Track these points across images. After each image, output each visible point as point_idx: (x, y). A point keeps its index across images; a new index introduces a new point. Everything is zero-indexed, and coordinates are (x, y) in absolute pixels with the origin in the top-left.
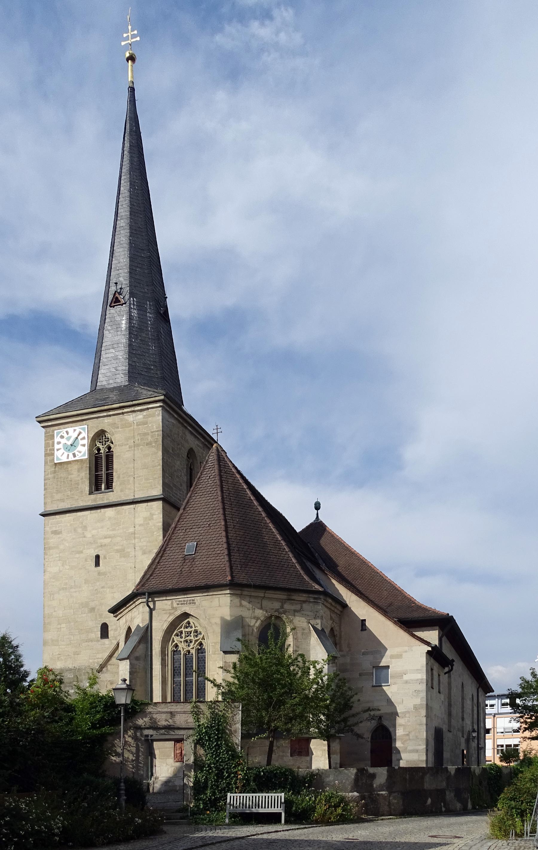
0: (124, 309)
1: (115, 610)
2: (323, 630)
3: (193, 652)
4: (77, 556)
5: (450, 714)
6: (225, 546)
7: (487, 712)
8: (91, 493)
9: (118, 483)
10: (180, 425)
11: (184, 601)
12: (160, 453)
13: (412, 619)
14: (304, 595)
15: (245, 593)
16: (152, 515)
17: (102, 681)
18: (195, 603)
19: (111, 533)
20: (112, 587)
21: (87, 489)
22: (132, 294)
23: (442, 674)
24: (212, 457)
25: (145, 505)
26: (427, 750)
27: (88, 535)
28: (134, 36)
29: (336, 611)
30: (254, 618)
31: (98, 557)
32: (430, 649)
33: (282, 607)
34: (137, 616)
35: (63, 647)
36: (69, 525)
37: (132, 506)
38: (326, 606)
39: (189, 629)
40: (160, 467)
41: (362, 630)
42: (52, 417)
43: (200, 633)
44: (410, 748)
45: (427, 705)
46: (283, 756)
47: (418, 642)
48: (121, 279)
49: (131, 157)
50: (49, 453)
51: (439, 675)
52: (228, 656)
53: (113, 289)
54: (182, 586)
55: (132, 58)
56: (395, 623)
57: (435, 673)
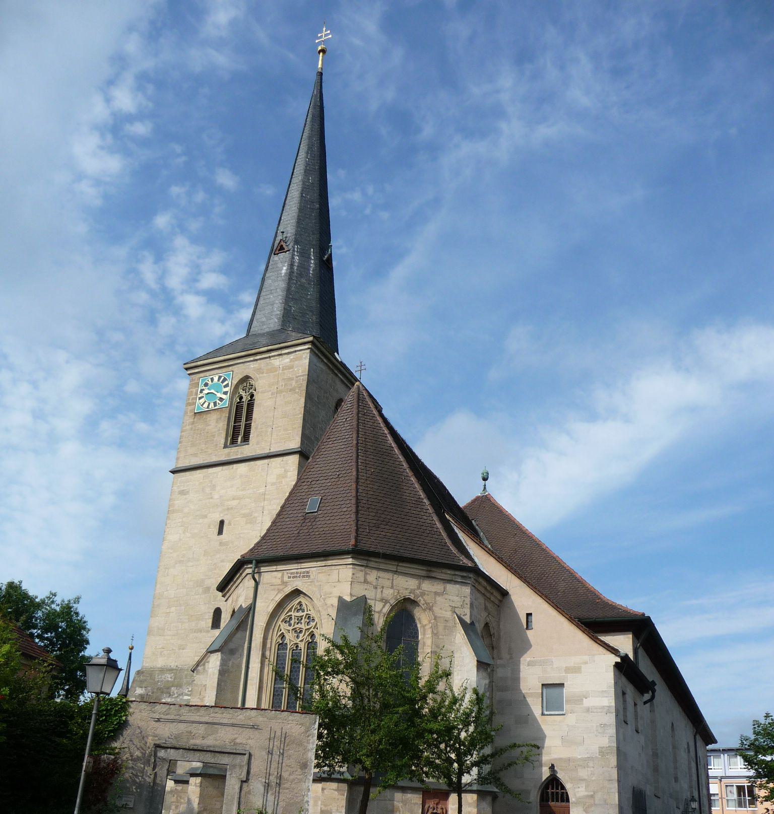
0: (287, 255)
2: (472, 623)
3: (302, 645)
4: (201, 521)
5: (656, 769)
6: (354, 501)
7: (710, 775)
8: (225, 446)
10: (328, 371)
11: (297, 573)
12: (303, 400)
13: (598, 621)
14: (449, 572)
15: (372, 564)
16: (286, 471)
18: (309, 576)
21: (223, 441)
22: (296, 242)
24: (350, 397)
27: (216, 496)
28: (326, 35)
29: (492, 598)
30: (382, 600)
31: (222, 523)
32: (619, 660)
33: (419, 587)
35: (169, 638)
37: (266, 461)
38: (478, 590)
39: (300, 614)
40: (301, 416)
41: (527, 628)
45: (618, 748)
47: (601, 649)
48: (289, 229)
51: (635, 704)
53: (279, 238)
56: (571, 619)
57: (630, 698)
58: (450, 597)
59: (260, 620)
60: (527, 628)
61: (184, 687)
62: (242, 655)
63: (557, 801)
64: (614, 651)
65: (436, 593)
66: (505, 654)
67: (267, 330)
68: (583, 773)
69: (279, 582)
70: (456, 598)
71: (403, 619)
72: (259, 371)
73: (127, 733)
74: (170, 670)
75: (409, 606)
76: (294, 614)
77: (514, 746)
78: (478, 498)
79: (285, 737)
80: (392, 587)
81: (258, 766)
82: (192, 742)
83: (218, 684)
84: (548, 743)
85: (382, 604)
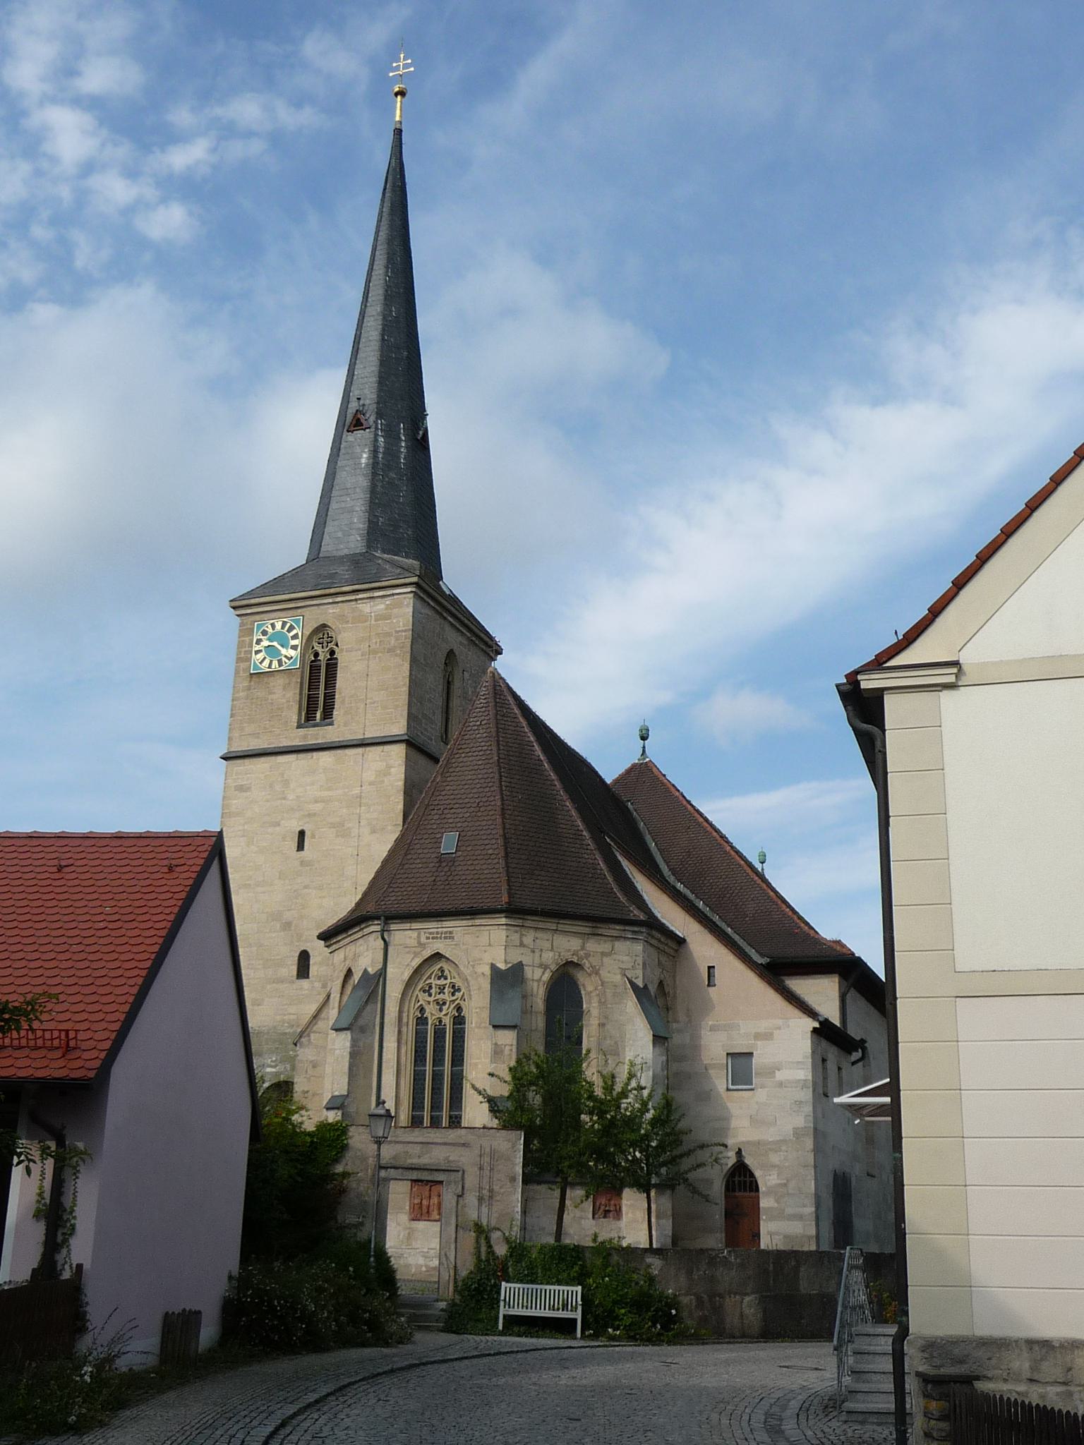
1: (327, 936)
2: (646, 986)
4: (270, 830)
6: (501, 841)
9: (342, 711)
12: (407, 666)
15: (528, 923)
17: (301, 1061)
19: (326, 793)
20: (320, 888)
21: (295, 718)
22: (380, 415)
23: (846, 1066)
25: (380, 748)
26: (817, 1218)
27: (291, 797)
28: (406, 66)
30: (541, 966)
32: (817, 1025)
33: (583, 948)
34: (364, 952)
36: (262, 776)
40: (406, 689)
41: (709, 985)
42: (253, 601)
43: (459, 990)
44: (789, 1211)
45: (815, 1129)
46: (581, 1218)
48: (366, 391)
49: (392, 221)
50: (243, 657)
51: (839, 1069)
52: (500, 1033)
54: (435, 907)
55: (402, 93)
57: (832, 1066)
58: (620, 957)
59: (394, 991)
60: (709, 985)
62: (373, 1033)
63: (745, 1190)
64: (810, 1012)
65: (603, 954)
66: (682, 1017)
67: (346, 552)
68: (775, 1158)
69: (414, 942)
70: (626, 958)
71: (565, 989)
72: (342, 618)
73: (349, 1155)
75: (571, 970)
76: (434, 982)
77: (702, 1147)
78: (634, 766)
79: (493, 1153)
80: (552, 950)
81: (471, 1181)
82: (409, 1161)
83: (350, 1069)
84: (734, 1123)
85: (541, 971)
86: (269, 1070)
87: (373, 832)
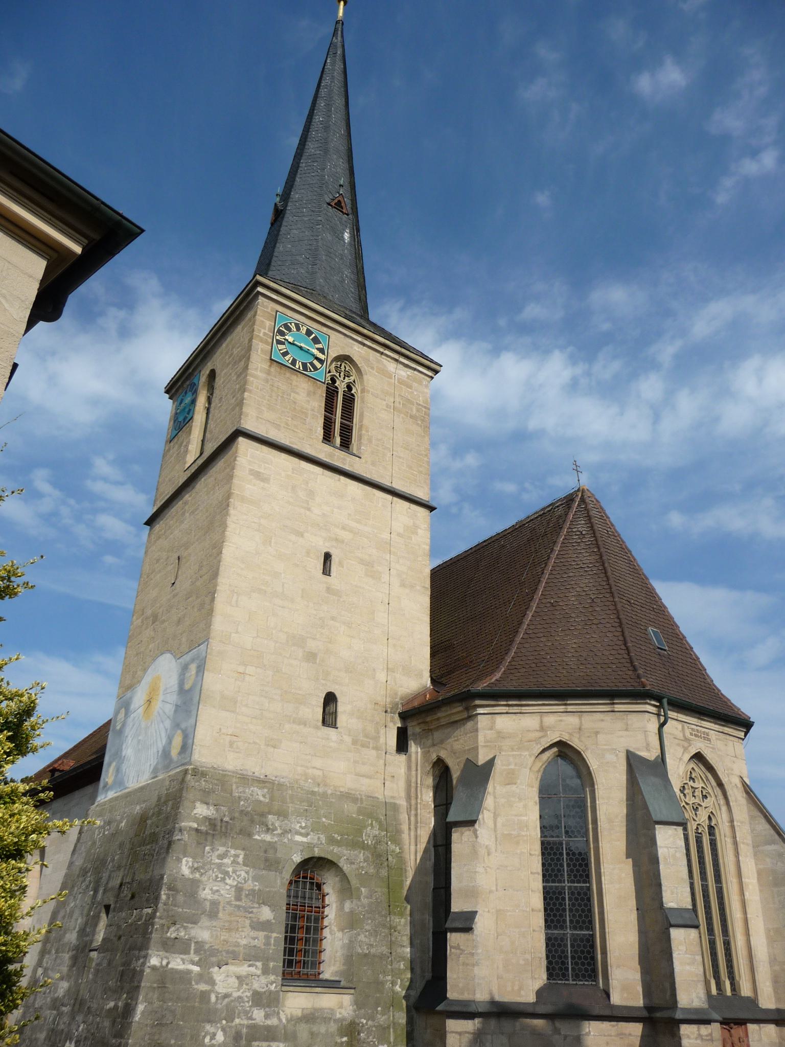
4: (293, 537)
61: (293, 818)
74: (262, 782)
76: (699, 784)
86: (298, 838)
87: (403, 585)
